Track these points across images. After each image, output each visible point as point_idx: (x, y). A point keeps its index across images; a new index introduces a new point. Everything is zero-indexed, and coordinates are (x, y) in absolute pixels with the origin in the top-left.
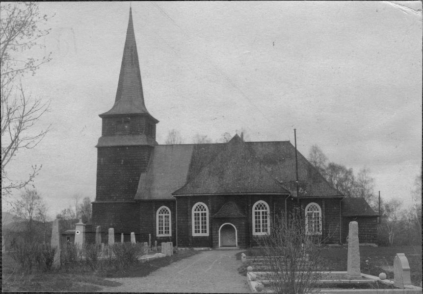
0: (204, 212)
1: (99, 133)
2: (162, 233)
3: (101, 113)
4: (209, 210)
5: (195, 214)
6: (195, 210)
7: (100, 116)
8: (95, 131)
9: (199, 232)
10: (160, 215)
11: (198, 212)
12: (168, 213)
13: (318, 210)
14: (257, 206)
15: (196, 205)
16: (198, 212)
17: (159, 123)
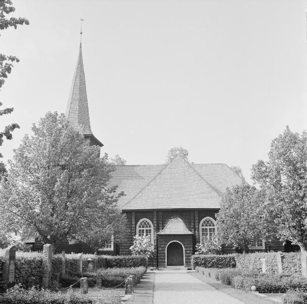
0: (148, 229)
6: (140, 227)
11: (206, 227)
12: (150, 227)
13: (150, 227)
15: (141, 220)
16: (206, 227)
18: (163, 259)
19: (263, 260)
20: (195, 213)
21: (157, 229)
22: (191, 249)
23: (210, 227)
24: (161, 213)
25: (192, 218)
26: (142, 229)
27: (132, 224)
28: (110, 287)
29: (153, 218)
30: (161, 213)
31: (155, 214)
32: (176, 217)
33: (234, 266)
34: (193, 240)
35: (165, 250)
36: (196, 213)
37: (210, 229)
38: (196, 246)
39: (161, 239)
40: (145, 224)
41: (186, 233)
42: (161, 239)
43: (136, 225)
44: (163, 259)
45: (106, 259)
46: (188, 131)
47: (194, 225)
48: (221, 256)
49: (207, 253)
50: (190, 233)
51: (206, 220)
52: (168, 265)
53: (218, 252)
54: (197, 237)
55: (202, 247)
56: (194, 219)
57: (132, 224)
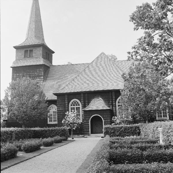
0: (78, 106)
1: (14, 59)
2: (52, 121)
3: (14, 46)
4: (82, 105)
6: (72, 106)
7: (15, 47)
8: (10, 59)
10: (72, 107)
11: (74, 107)
12: (79, 105)
13: (79, 105)
15: (72, 101)
16: (74, 107)
17: (55, 53)
18: (87, 129)
19: (160, 129)
20: (113, 93)
21: (84, 106)
22: (109, 120)
23: (77, 106)
24: (86, 95)
25: (110, 97)
26: (73, 107)
27: (65, 104)
28: (36, 150)
29: (81, 99)
30: (86, 95)
31: (82, 95)
32: (98, 97)
33: (139, 134)
34: (111, 113)
35: (89, 122)
36: (113, 93)
37: (76, 108)
38: (113, 119)
39: (87, 113)
40: (75, 103)
41: (105, 109)
42: (87, 113)
43: (68, 104)
44: (87, 129)
45: (35, 131)
46: (99, 39)
47: (112, 103)
48: (128, 126)
49: (120, 123)
50: (109, 108)
51: (74, 102)
52: (92, 133)
53: (130, 122)
54: (114, 111)
55: (117, 119)
56: (112, 98)
57: (65, 104)
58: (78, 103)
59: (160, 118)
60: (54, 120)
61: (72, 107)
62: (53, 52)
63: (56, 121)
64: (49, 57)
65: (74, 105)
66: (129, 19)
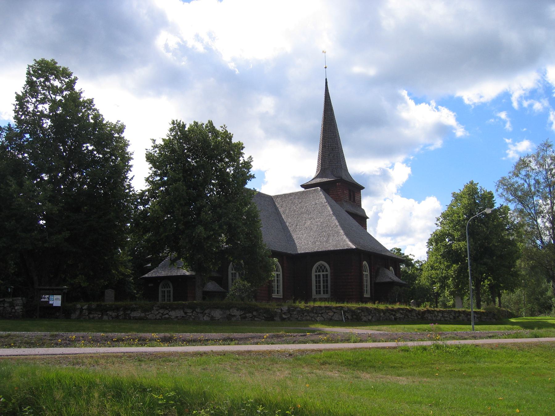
0: (325, 273)
5: (316, 275)
9: (320, 293)
11: (319, 273)
12: (327, 271)
13: (327, 271)
14: (317, 268)
16: (319, 273)
37: (323, 275)
58: (325, 267)
59: (318, 297)
60: (324, 291)
61: (326, 273)
62: (363, 188)
63: (327, 293)
64: (354, 199)
65: (319, 271)
66: (503, 176)
